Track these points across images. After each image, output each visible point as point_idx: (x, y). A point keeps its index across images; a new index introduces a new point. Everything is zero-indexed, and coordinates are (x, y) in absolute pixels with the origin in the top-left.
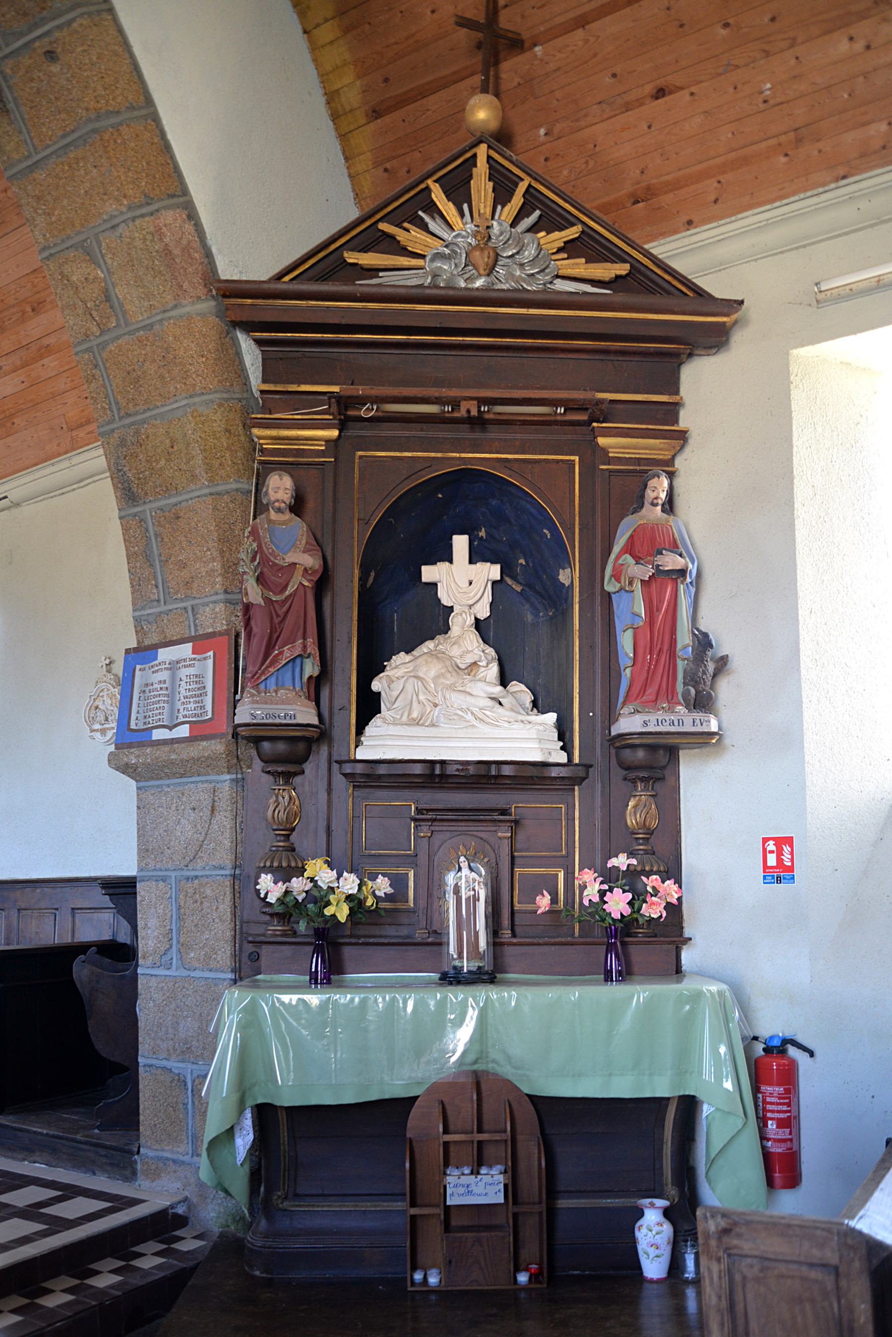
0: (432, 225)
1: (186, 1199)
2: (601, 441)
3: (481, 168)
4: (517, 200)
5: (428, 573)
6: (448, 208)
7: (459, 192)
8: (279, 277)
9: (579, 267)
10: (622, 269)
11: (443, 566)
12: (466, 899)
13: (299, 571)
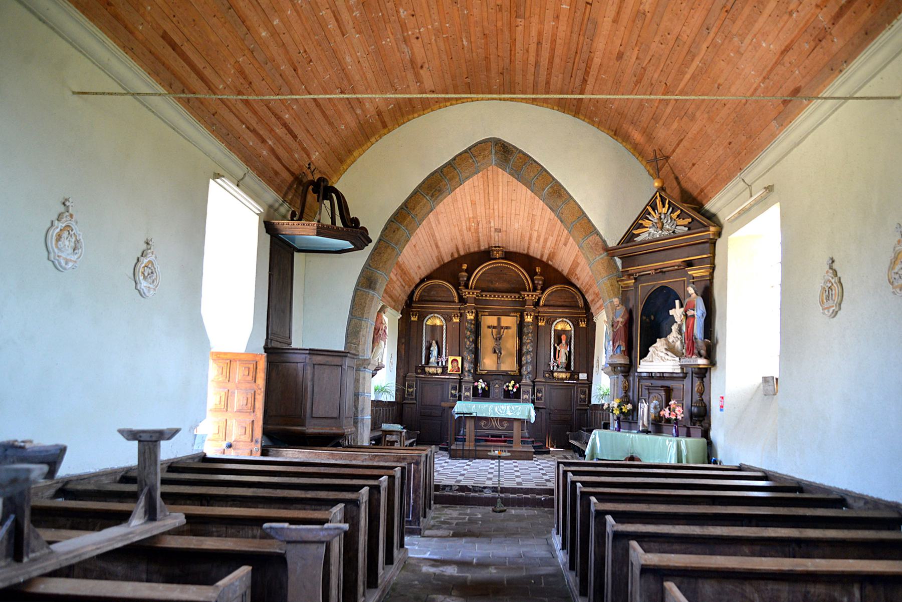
4: (667, 206)
5: (671, 312)
6: (652, 212)
7: (654, 208)
9: (681, 222)
10: (690, 220)
13: (620, 324)
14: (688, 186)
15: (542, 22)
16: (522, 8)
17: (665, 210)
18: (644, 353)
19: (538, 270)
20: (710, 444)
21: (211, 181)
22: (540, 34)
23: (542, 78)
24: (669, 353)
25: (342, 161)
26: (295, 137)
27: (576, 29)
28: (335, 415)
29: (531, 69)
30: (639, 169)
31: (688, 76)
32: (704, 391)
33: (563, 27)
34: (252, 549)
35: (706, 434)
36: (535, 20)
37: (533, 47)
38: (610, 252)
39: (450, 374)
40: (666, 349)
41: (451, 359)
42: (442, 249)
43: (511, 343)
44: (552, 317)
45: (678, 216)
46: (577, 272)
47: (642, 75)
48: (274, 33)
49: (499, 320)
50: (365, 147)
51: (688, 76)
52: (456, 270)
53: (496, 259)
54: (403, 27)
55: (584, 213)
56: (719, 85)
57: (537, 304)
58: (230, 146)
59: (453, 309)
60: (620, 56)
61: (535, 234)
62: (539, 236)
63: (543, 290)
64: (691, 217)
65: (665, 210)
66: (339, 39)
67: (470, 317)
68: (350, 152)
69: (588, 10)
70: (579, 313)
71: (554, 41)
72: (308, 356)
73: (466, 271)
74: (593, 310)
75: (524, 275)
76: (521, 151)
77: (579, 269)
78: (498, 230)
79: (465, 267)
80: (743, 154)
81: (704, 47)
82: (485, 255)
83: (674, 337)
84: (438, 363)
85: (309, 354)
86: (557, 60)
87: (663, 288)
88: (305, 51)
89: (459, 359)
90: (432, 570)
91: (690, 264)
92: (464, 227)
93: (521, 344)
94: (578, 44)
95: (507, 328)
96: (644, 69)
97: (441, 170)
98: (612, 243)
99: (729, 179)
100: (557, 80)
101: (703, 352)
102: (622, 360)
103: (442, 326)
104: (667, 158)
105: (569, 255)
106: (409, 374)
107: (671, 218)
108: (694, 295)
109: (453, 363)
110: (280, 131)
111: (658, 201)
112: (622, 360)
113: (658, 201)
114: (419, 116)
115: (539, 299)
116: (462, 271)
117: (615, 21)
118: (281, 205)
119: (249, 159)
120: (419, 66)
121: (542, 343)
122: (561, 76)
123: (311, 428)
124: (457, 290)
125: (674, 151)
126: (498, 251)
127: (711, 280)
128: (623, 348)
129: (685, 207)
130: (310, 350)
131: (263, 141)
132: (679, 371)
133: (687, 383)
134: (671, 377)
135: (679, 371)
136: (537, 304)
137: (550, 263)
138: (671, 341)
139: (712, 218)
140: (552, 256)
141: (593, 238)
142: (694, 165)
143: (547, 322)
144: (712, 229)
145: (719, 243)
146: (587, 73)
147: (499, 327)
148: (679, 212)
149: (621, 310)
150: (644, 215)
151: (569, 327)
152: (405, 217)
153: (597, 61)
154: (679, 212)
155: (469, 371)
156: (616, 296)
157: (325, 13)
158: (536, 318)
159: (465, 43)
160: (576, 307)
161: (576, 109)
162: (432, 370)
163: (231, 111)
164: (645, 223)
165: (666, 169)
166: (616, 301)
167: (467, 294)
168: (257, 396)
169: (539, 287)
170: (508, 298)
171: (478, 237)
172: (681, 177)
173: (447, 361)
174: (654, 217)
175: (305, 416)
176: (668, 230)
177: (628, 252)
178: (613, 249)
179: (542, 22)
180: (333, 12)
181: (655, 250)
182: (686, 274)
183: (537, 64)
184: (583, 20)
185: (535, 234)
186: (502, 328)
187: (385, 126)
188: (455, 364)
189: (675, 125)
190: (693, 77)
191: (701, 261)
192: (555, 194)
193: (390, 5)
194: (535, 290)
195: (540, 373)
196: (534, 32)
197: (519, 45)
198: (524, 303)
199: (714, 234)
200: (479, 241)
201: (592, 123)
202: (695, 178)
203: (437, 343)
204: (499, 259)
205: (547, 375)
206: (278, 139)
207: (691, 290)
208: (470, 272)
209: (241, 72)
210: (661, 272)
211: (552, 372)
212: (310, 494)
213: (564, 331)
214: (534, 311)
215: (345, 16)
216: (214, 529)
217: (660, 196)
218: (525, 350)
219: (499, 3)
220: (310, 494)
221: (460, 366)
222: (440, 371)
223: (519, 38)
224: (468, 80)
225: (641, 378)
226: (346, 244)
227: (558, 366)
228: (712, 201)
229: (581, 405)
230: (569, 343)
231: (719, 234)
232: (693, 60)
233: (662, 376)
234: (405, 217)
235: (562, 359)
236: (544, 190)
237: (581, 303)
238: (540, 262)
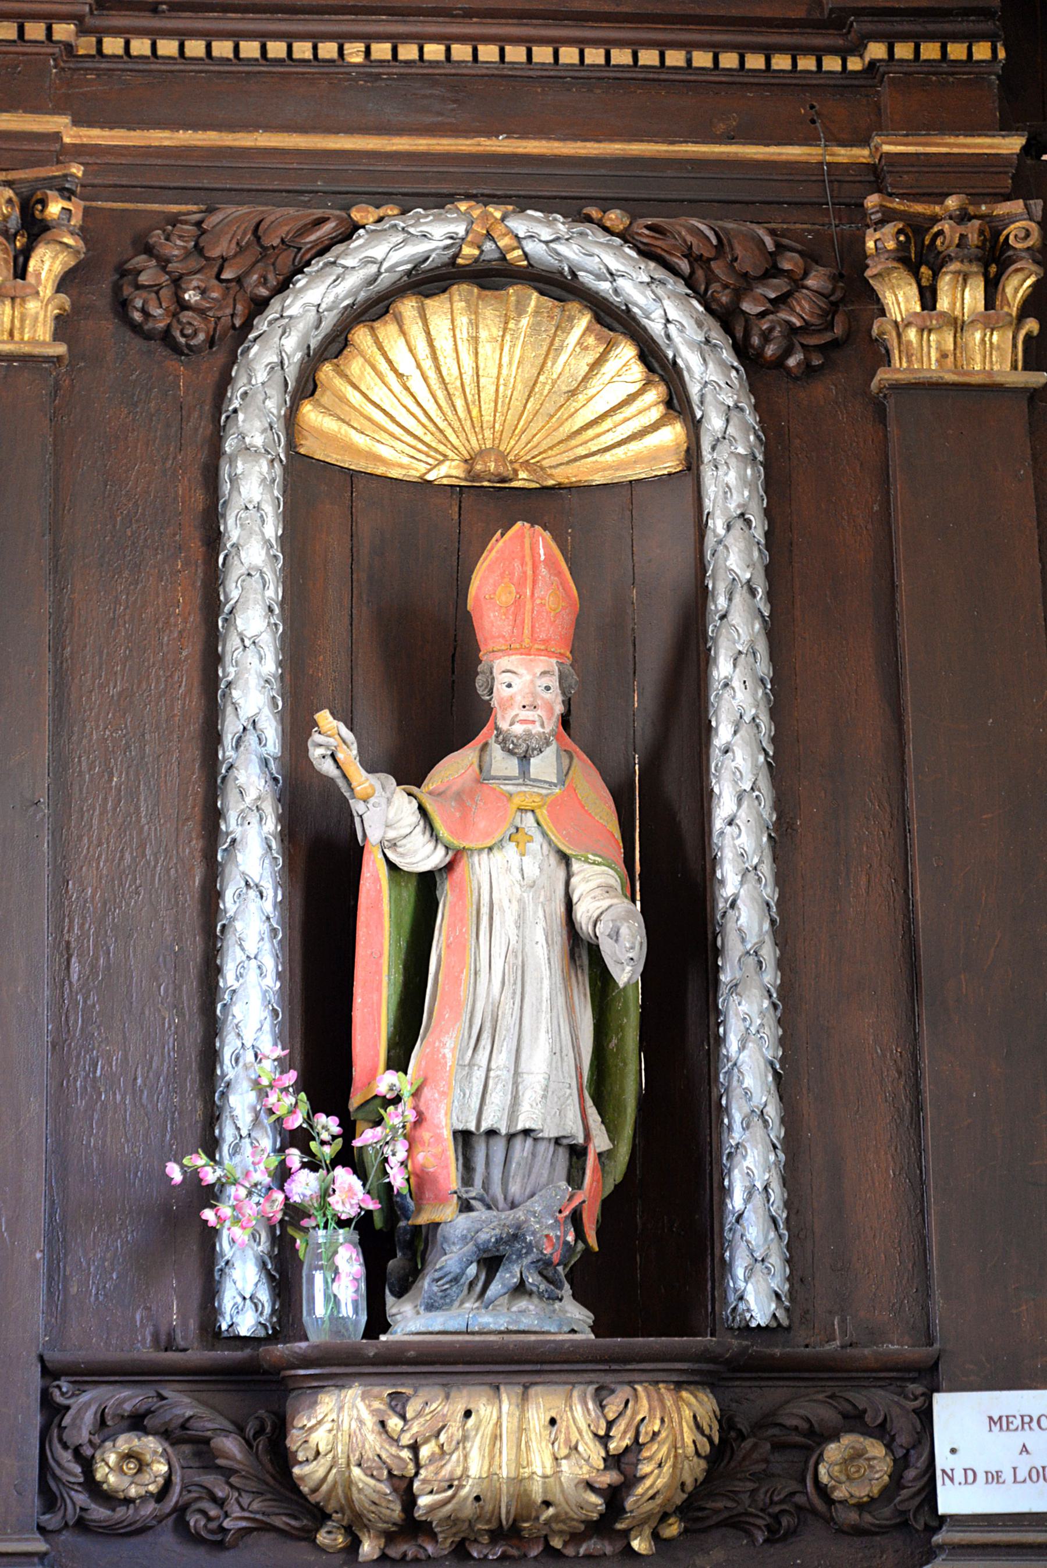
143: (102, 286)
227: (393, 1246)
235: (506, 1058)
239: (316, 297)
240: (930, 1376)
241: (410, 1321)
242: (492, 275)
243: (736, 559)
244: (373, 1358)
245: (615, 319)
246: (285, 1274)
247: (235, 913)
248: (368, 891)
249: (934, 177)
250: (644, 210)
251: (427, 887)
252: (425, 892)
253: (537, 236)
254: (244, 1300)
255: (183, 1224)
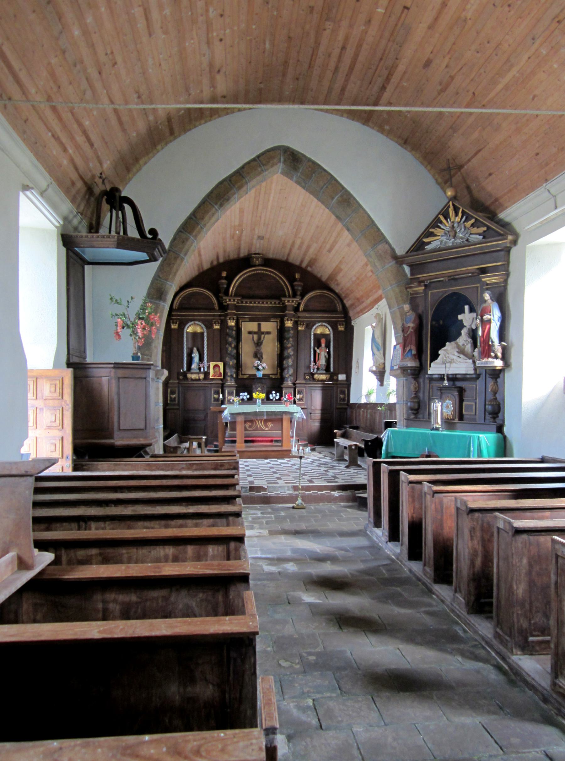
0: (442, 227)
1: (305, 374)
2: (483, 280)
3: (451, 207)
4: (460, 214)
5: (460, 317)
6: (444, 221)
7: (446, 217)
8: (407, 252)
9: (475, 230)
10: (485, 229)
11: (463, 315)
12: (203, 360)
13: (411, 328)
14: (480, 196)
15: (351, 26)
16: (334, 11)
17: (458, 219)
18: (435, 356)
19: (297, 276)
20: (505, 438)
21: (21, 193)
22: (347, 39)
23: (338, 86)
24: (461, 356)
25: (128, 170)
26: (92, 145)
27: (387, 34)
28: (142, 427)
29: (329, 74)
30: (425, 178)
31: (500, 86)
32: (497, 391)
33: (373, 31)
34: (216, 572)
35: (500, 429)
36: (345, 23)
37: (337, 51)
38: (398, 260)
39: (212, 380)
40: (458, 352)
41: (212, 364)
42: (203, 257)
43: (270, 346)
44: (311, 322)
45: (473, 225)
46: (339, 278)
47: (448, 85)
48: (86, 33)
49: (259, 326)
50: (151, 155)
51: (500, 86)
52: (214, 278)
53: (255, 266)
54: (209, 25)
55: (373, 222)
56: (534, 97)
57: (296, 309)
58: (37, 155)
59: (214, 316)
60: (428, 63)
61: (298, 242)
62: (302, 243)
63: (303, 296)
64: (485, 225)
65: (458, 219)
66: (145, 39)
67: (232, 323)
68: (137, 160)
69: (404, 15)
70: (338, 317)
71: (359, 46)
72: (113, 370)
73: (226, 278)
74: (351, 314)
75: (284, 281)
76: (310, 160)
77: (341, 274)
78: (261, 238)
79: (224, 274)
80: (552, 165)
81: (526, 57)
82: (245, 262)
83: (464, 339)
84: (200, 369)
85: (114, 367)
86: (358, 66)
87: (455, 294)
88: (112, 53)
89: (221, 365)
90: (273, 569)
91: (483, 271)
92: (228, 235)
93: (282, 348)
94: (385, 51)
95: (268, 333)
96: (452, 78)
97: (230, 178)
98: (400, 251)
99: (532, 188)
100: (353, 88)
101: (499, 355)
102: (411, 363)
103: (202, 334)
104: (460, 167)
105: (345, 261)
106: (171, 381)
107: (465, 227)
108: (490, 301)
109: (215, 368)
110: (80, 139)
111: (451, 210)
112: (411, 363)
113: (451, 210)
114: (206, 122)
115: (299, 304)
116: (222, 278)
117: (430, 27)
118: (75, 216)
119: (52, 169)
120: (217, 70)
121: (302, 346)
122: (359, 83)
123: (119, 441)
124: (217, 297)
125: (469, 160)
126: (257, 259)
127: (505, 287)
128: (414, 352)
129: (480, 217)
130: (115, 364)
131: (65, 150)
132: (472, 372)
133: (480, 383)
134: (464, 378)
135: (472, 372)
136: (296, 309)
137: (309, 269)
138: (461, 344)
139: (505, 225)
140: (312, 262)
141: (382, 247)
142: (490, 174)
144: (510, 237)
145: (514, 251)
146: (388, 80)
147: (259, 333)
148: (473, 221)
149: (412, 316)
150: (436, 223)
151: (328, 330)
152: (191, 225)
153: (401, 68)
154: (473, 221)
155: (232, 376)
156: (404, 303)
157: (138, 11)
158: (296, 323)
159: (267, 46)
160: (334, 311)
161: (366, 119)
162: (194, 376)
163: (40, 118)
164: (437, 231)
165: (457, 179)
166: (407, 307)
167: (228, 301)
168: (65, 412)
169: (299, 293)
170: (267, 304)
171: (240, 245)
172: (473, 186)
173: (209, 367)
174: (446, 225)
175: (113, 429)
176: (462, 238)
177: (417, 260)
178: (402, 257)
179: (351, 26)
180: (145, 10)
181: (445, 258)
182: (480, 281)
183: (337, 69)
184: (396, 25)
185: (298, 242)
186: (263, 333)
187: (172, 132)
188: (217, 369)
189: (476, 135)
190: (506, 88)
191: (495, 269)
192: (342, 201)
193: (200, 4)
194: (294, 295)
195: (301, 375)
196: (341, 37)
197: (322, 49)
198: (284, 308)
199: (511, 242)
200: (239, 248)
201: (381, 130)
202: (492, 187)
203: (198, 350)
204: (259, 265)
205: (307, 377)
206: (77, 147)
207: (487, 296)
208: (230, 279)
209: (53, 75)
210: (454, 279)
211: (312, 375)
212: (192, 509)
213: (326, 336)
214: (294, 316)
215: (155, 15)
216: (124, 551)
217: (453, 205)
218: (286, 354)
219: (312, 4)
220: (192, 509)
221: (222, 371)
222: (202, 376)
223: (324, 41)
224: (262, 86)
225: (431, 379)
226: (143, 256)
227: (318, 369)
228: (508, 211)
229: (340, 404)
230: (328, 346)
231: (515, 242)
232: (509, 70)
233: (453, 379)
234: (191, 225)
236: (333, 198)
237: (339, 307)
238: (299, 268)
239: (314, 327)
240: (339, 374)
241: (319, 372)
242: (322, 325)
243: (332, 339)
244: (317, 373)
245: (327, 327)
246: (313, 370)
247: (360, 466)
248: (99, 632)
249: (340, 321)
250: (329, 323)
251: (319, 354)
252: (319, 354)
253: (324, 324)
254: (312, 371)
255: (309, 368)
